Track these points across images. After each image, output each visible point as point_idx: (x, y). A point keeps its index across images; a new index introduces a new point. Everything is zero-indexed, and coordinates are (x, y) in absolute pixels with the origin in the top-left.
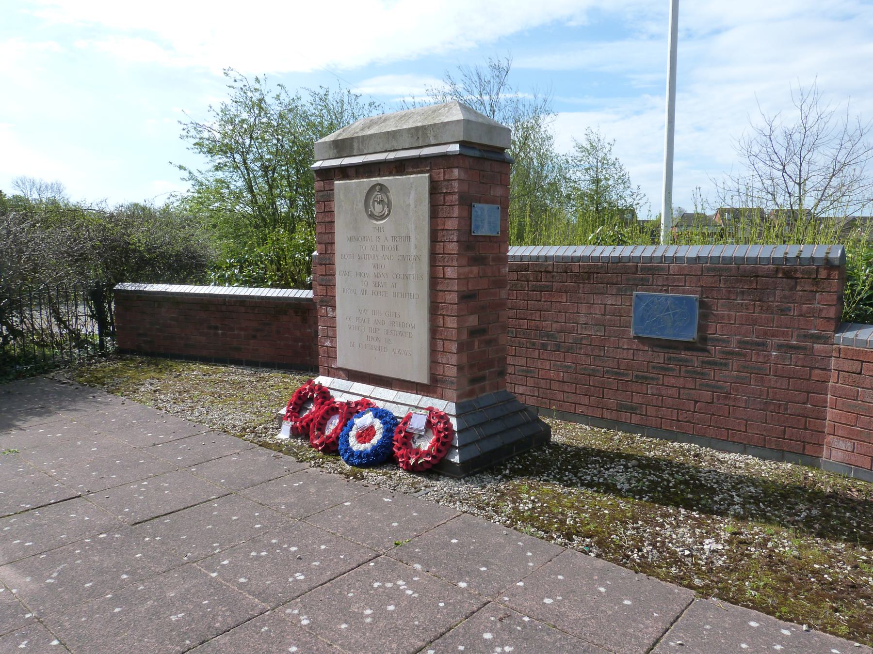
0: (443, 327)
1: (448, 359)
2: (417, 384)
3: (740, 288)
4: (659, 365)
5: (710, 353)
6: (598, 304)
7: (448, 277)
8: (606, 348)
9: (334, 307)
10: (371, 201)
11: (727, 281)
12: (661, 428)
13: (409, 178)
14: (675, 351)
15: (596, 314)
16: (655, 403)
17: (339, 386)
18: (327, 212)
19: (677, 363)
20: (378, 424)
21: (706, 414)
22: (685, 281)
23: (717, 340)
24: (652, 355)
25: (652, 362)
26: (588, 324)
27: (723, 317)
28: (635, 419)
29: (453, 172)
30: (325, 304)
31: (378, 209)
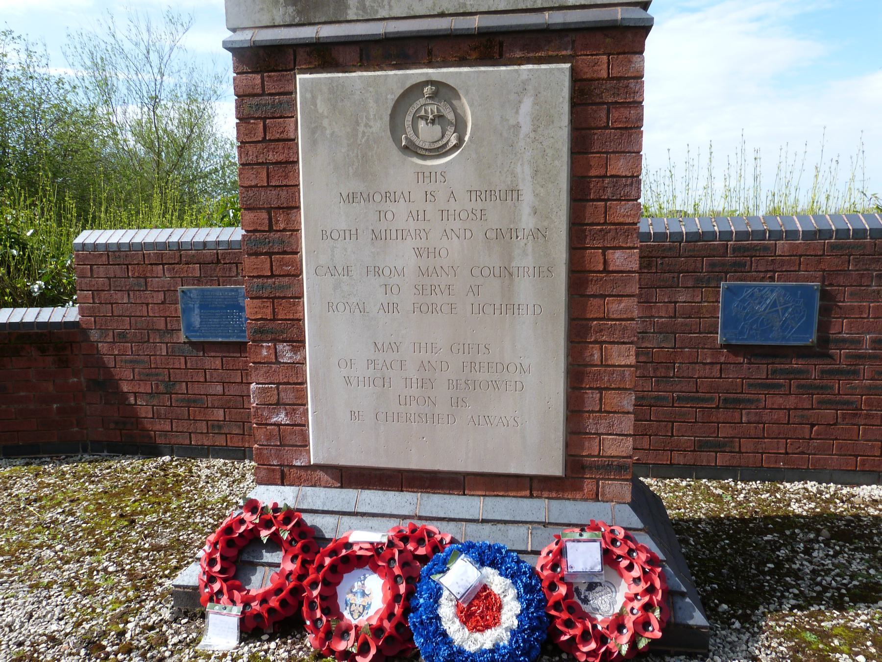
0: (602, 365)
1: (611, 426)
2: (531, 478)
3: (877, 271)
4: (760, 381)
5: (834, 360)
6: (665, 302)
7: (617, 269)
8: (677, 365)
9: (298, 343)
10: (409, 118)
11: (859, 262)
12: (762, 466)
13: (517, 71)
14: (783, 360)
15: (662, 317)
16: (752, 434)
17: (324, 504)
18: (270, 140)
19: (786, 377)
20: (498, 583)
21: (826, 439)
22: (800, 264)
23: (844, 340)
24: (749, 369)
25: (748, 378)
26: (646, 333)
27: (852, 308)
28: (722, 459)
29: (630, 61)
30: (270, 337)
31: (427, 133)
